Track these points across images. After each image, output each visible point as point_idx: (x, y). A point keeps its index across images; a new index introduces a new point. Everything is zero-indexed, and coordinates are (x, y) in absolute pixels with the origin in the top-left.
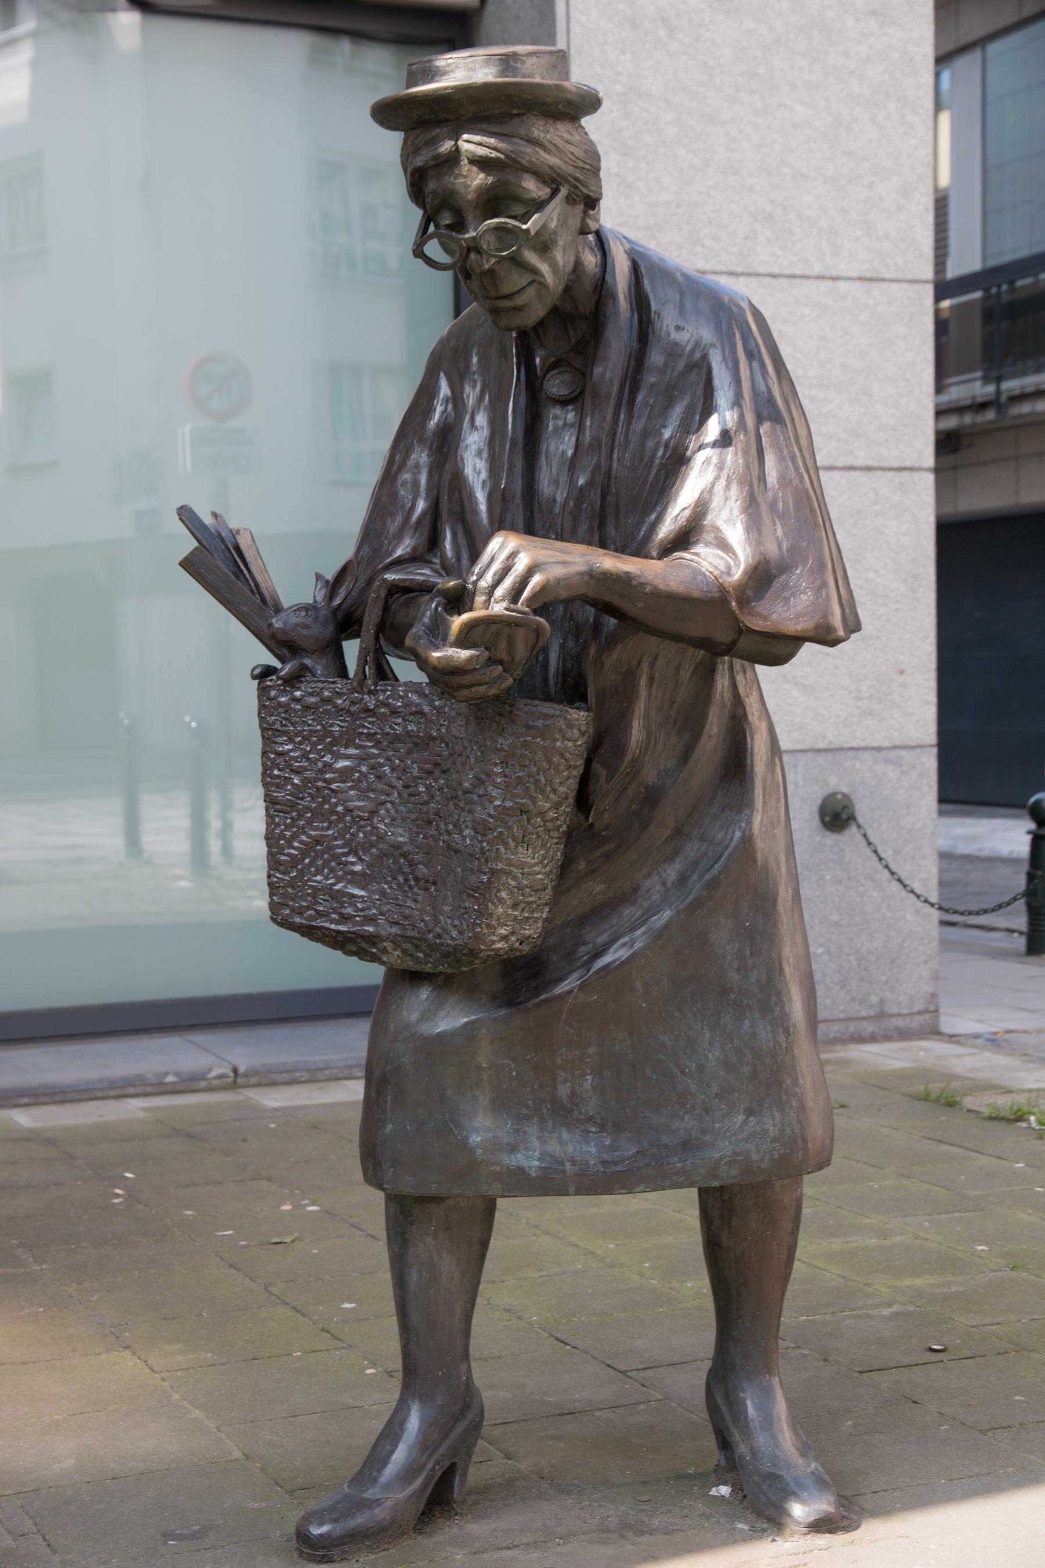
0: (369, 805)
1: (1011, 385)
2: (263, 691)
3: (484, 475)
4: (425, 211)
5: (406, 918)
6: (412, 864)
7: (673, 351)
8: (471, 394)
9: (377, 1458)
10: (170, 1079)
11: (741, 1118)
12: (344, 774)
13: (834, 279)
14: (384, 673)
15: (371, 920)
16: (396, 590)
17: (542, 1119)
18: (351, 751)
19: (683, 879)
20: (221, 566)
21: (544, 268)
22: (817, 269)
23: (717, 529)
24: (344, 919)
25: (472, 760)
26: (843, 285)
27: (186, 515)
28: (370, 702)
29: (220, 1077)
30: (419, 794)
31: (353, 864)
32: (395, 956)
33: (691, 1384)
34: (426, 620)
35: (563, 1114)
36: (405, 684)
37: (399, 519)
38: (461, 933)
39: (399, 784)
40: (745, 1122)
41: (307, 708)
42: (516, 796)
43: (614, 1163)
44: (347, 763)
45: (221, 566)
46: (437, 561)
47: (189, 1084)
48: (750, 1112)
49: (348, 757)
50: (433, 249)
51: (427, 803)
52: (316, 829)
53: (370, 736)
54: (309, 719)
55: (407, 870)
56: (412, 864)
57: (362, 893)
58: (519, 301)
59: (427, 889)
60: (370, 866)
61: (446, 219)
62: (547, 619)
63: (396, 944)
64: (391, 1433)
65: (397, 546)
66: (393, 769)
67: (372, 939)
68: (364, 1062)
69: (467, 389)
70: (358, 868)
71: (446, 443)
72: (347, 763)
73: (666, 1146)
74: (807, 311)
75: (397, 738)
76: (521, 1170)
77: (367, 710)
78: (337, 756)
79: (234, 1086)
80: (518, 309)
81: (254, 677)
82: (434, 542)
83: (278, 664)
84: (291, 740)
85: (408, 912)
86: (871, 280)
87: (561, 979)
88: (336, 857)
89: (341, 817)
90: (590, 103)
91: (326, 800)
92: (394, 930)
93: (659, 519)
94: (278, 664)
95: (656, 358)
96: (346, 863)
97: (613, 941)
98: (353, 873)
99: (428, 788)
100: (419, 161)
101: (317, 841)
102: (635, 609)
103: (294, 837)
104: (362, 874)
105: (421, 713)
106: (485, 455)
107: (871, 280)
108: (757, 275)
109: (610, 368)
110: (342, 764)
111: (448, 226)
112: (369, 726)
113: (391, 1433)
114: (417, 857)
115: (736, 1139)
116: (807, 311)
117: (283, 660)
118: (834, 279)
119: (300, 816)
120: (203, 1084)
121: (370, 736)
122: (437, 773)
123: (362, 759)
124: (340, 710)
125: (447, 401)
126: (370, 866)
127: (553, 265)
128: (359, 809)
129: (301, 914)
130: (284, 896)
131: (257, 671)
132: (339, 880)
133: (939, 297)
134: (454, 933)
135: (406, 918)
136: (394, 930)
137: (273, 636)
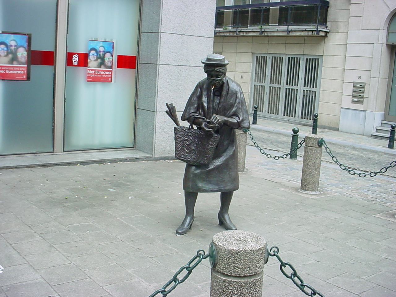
1: (239, 29)
7: (232, 91)
9: (183, 223)
12: (186, 140)
15: (189, 158)
18: (187, 137)
23: (237, 114)
28: (191, 131)
38: (203, 161)
41: (182, 131)
54: (182, 133)
57: (188, 155)
60: (189, 152)
62: (205, 130)
64: (185, 220)
68: (327, 22)
70: (188, 152)
71: (200, 97)
77: (190, 132)
78: (186, 138)
88: (185, 150)
91: (184, 143)
93: (230, 112)
101: (182, 148)
103: (179, 147)
104: (188, 153)
108: (352, 133)
109: (224, 93)
110: (186, 139)
113: (185, 220)
115: (228, 187)
119: (180, 145)
123: (189, 138)
124: (186, 132)
132: (185, 153)
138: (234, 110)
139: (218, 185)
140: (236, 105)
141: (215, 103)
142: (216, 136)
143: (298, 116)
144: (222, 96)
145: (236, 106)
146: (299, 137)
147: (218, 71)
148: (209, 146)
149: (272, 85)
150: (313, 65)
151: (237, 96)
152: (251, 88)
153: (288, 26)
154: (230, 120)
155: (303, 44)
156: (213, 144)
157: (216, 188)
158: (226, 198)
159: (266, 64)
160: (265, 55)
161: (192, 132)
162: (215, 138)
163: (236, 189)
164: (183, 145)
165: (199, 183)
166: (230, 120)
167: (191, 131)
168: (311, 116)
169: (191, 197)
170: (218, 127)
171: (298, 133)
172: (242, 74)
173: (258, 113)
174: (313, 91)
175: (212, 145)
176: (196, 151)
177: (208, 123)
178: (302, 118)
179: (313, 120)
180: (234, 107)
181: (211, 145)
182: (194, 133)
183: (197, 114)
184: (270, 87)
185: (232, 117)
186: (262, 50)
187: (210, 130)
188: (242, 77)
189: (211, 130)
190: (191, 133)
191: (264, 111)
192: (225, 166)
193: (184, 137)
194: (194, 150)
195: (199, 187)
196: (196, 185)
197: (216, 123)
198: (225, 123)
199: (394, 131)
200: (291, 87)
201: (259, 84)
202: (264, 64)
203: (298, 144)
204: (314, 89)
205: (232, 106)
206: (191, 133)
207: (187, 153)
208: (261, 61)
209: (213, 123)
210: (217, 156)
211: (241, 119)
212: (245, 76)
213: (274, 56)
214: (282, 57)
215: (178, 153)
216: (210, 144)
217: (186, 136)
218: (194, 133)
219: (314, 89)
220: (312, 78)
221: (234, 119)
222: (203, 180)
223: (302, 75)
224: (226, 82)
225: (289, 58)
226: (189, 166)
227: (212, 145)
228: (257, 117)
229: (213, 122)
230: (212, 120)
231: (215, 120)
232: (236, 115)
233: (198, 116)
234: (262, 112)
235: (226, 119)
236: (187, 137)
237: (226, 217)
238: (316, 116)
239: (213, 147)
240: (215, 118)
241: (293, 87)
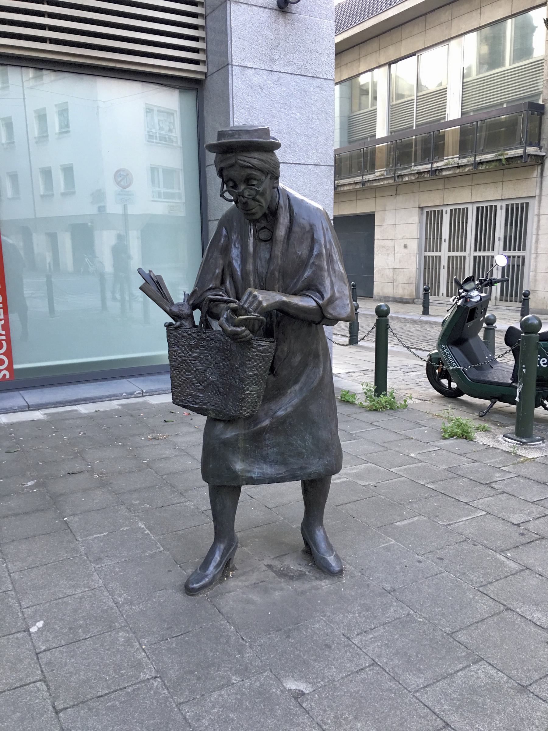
0: (204, 368)
2: (168, 331)
3: (239, 263)
4: (223, 179)
5: (216, 404)
6: (218, 388)
8: (234, 237)
10: (124, 394)
11: (317, 460)
13: (307, 165)
14: (208, 326)
15: (205, 404)
16: (211, 300)
17: (258, 461)
19: (301, 389)
20: (155, 288)
21: (262, 200)
22: (303, 162)
23: (316, 286)
24: (196, 403)
25: (239, 358)
26: (310, 166)
27: (140, 271)
28: (204, 336)
29: (138, 393)
30: (221, 366)
31: (199, 386)
32: (213, 415)
33: (297, 524)
34: (225, 316)
35: (265, 459)
36: (215, 331)
37: (211, 275)
38: (235, 411)
39: (214, 362)
40: (319, 461)
41: (184, 337)
42: (254, 371)
43: (280, 474)
44: (196, 355)
45: (155, 288)
46: (223, 289)
47: (130, 395)
48: (320, 458)
49: (197, 353)
50: (227, 195)
51: (223, 369)
52: (187, 375)
53: (203, 347)
55: (217, 389)
56: (218, 388)
58: (253, 211)
59: (223, 396)
61: (231, 184)
63: (214, 412)
64: (212, 552)
65: (210, 284)
66: (211, 358)
67: (207, 410)
69: (233, 234)
71: (226, 251)
72: (196, 355)
73: (295, 469)
74: (300, 174)
75: (212, 348)
76: (252, 477)
77: (202, 338)
78: (193, 352)
79: (143, 396)
80: (254, 214)
81: (165, 326)
82: (223, 282)
83: (174, 323)
84: (178, 347)
85: (217, 402)
86: (317, 165)
87: (264, 421)
88: (193, 384)
89: (195, 372)
90: (278, 146)
92: (213, 408)
93: (298, 281)
94: (174, 323)
95: (296, 229)
96: (197, 386)
97: (280, 408)
98: (199, 389)
99: (223, 365)
100: (222, 165)
102: (291, 311)
104: (202, 390)
105: (221, 341)
106: (240, 257)
107: (317, 165)
109: (281, 232)
111: (232, 187)
112: (204, 343)
113: (212, 552)
114: (220, 386)
115: (315, 467)
116: (300, 174)
117: (176, 321)
118: (307, 165)
120: (133, 396)
121: (203, 347)
122: (226, 360)
125: (226, 236)
126: (204, 387)
127: (266, 200)
128: (201, 369)
129: (183, 401)
130: (177, 396)
131: (167, 324)
132: (195, 391)
133: (338, 174)
134: (233, 411)
135: (216, 404)
136: (213, 408)
137: (172, 313)
138: (308, 273)
139: (284, 463)
140: (311, 261)
141: (261, 260)
142: (263, 346)
143: (496, 298)
144: (276, 240)
145: (313, 263)
146: (497, 331)
147: (246, 164)
148: (246, 372)
149: (452, 254)
150: (518, 215)
151: (315, 237)
152: (420, 260)
153: (475, 156)
154: (296, 300)
155: (501, 183)
156: (254, 366)
157: (281, 470)
158: (315, 491)
159: (441, 223)
160: (440, 209)
161: (208, 337)
162: (259, 351)
163: (336, 468)
164: (188, 371)
165: (235, 462)
166: (296, 300)
167: (204, 336)
168: (516, 296)
169: (224, 489)
170: (262, 321)
171: (494, 325)
172: (406, 242)
173: (431, 297)
174: (519, 257)
175: (254, 368)
176: (220, 386)
177: (235, 311)
178: (501, 300)
179: (520, 302)
180: (309, 267)
181: (250, 369)
182: (212, 340)
183: (221, 293)
184: (449, 257)
185: (303, 292)
186: (432, 199)
187: (239, 329)
188: (405, 246)
189: (244, 331)
190: (205, 339)
191: (441, 294)
192: (302, 417)
193: (190, 350)
194: (213, 382)
195: (235, 472)
196: (229, 469)
197: (255, 312)
198: (283, 313)
199: (493, 329)
200: (482, 254)
201: (486, 254)
202: (438, 223)
203: (447, 385)
204: (521, 253)
205: (303, 264)
206: (205, 339)
207: (200, 391)
208: (432, 218)
209: (247, 312)
210: (273, 393)
211: (327, 296)
212: (409, 243)
213: (453, 207)
214: (467, 209)
215: (178, 392)
216: (248, 368)
217: (193, 348)
218: (212, 340)
219: (521, 253)
220: (516, 239)
221: (310, 299)
222: (246, 455)
223: (500, 232)
224: (285, 206)
225: (478, 208)
226: (212, 422)
227: (254, 368)
228: (429, 303)
229: (245, 309)
230: (245, 303)
231: (252, 303)
232: (313, 288)
233: (221, 297)
234: (438, 295)
235: (285, 299)
236: (198, 351)
237: (319, 534)
238: (526, 295)
239: (255, 375)
240: (251, 299)
241: (486, 254)
